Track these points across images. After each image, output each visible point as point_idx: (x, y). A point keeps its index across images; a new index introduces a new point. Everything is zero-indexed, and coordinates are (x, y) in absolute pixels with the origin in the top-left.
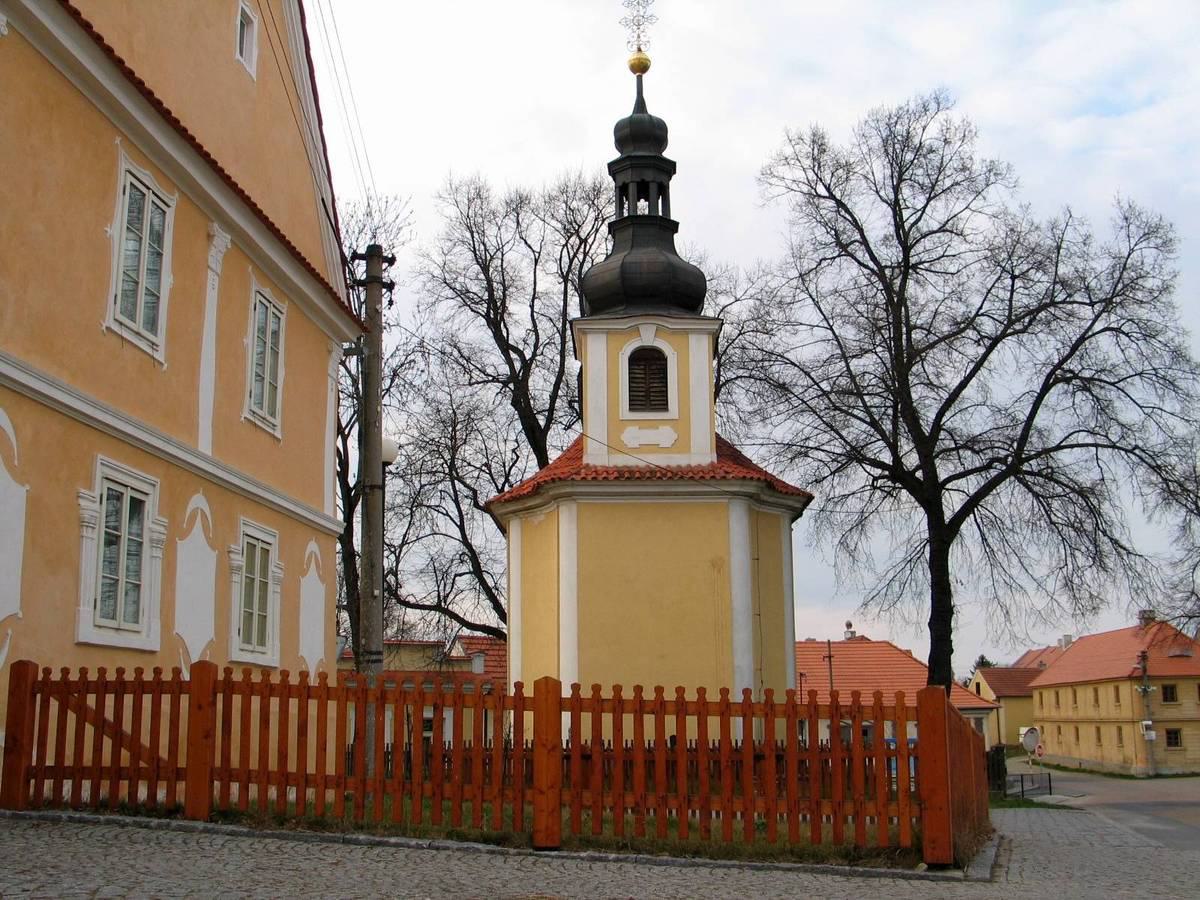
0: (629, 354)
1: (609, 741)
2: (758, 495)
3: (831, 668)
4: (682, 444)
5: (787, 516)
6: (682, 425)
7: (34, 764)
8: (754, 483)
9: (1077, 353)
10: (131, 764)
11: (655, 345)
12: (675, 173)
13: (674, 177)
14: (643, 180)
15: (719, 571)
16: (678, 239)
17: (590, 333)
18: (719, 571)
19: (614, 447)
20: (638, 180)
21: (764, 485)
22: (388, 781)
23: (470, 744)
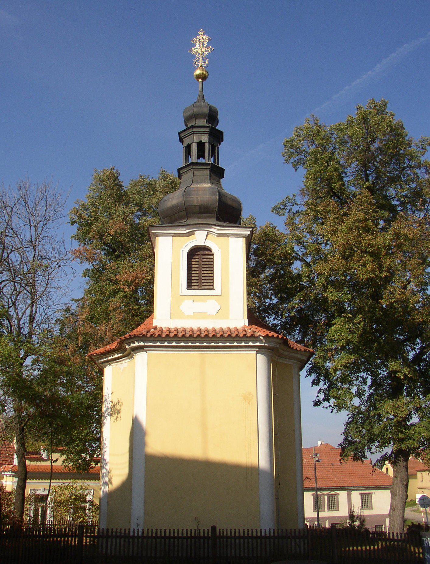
0: (187, 251)
1: (208, 530)
2: (277, 348)
3: (316, 481)
4: (222, 312)
5: (297, 365)
6: (223, 298)
7: (96, 534)
8: (275, 340)
9: (48, 503)
10: (386, 520)
11: (205, 245)
12: (223, 141)
13: (222, 143)
14: (201, 141)
15: (249, 403)
16: (222, 180)
17: (158, 236)
18: (249, 403)
19: (174, 313)
20: (198, 141)
21: (281, 341)
22: (85, 258)
23: (208, 533)
